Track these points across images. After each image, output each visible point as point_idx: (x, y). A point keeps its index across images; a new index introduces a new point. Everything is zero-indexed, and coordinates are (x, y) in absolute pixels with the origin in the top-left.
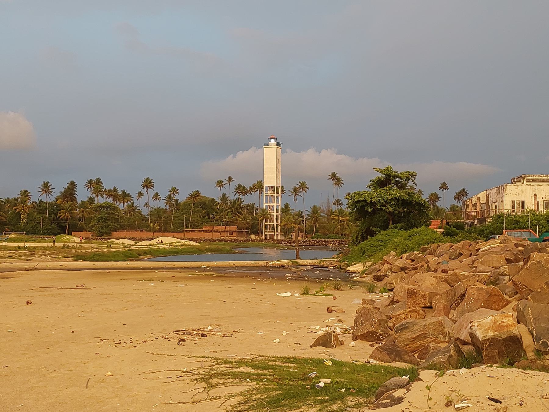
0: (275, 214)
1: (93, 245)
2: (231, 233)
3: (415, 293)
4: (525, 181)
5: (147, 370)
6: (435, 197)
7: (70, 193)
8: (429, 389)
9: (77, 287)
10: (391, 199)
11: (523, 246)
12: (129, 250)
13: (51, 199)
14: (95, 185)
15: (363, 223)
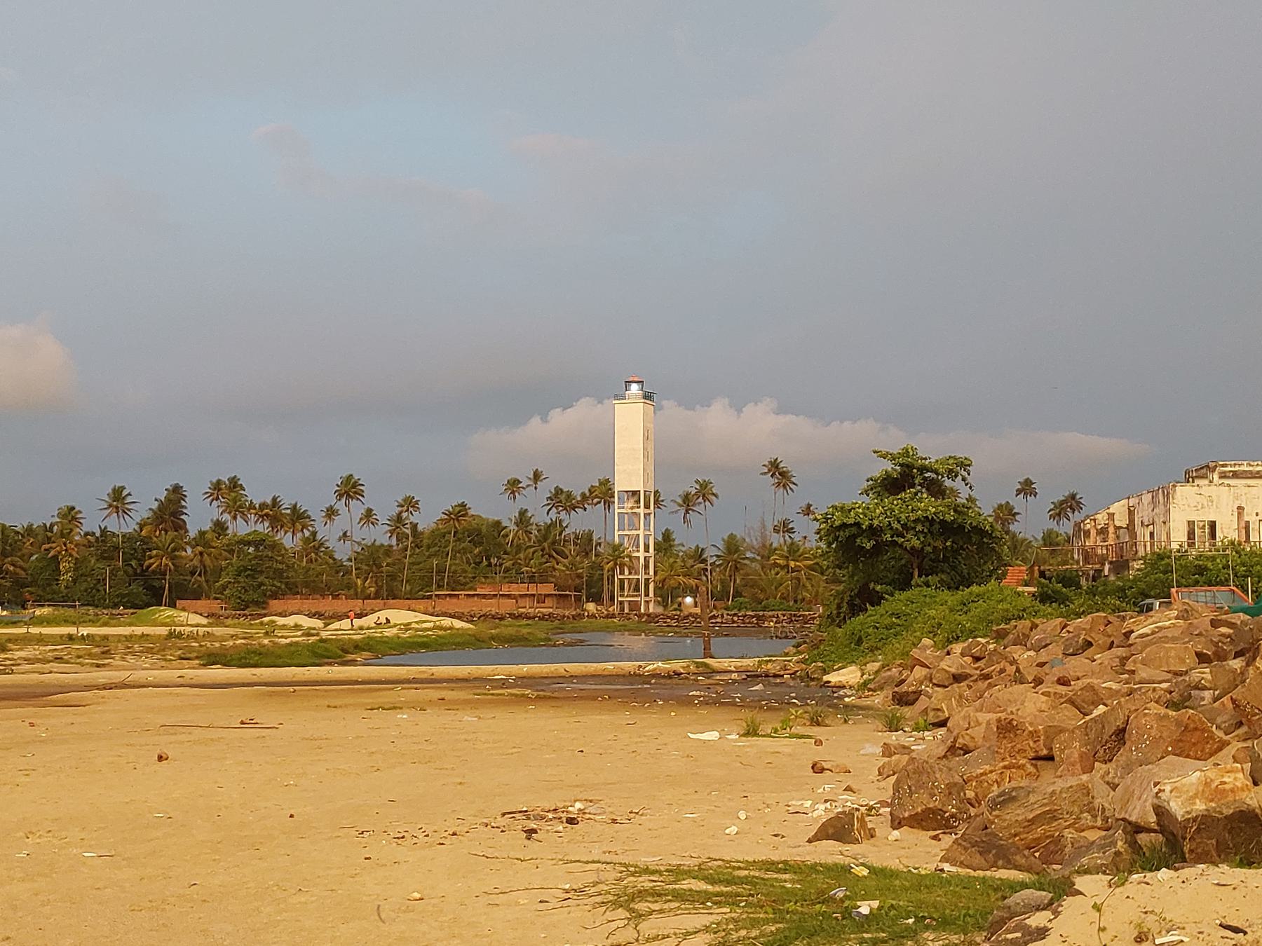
0: (641, 554)
1: (231, 631)
2: (541, 599)
3: (1015, 728)
4: (1216, 476)
5: (490, 889)
6: (1006, 513)
7: (171, 511)
8: (1099, 910)
9: (242, 723)
10: (917, 521)
11: (1231, 625)
12: (171, 635)
13: (123, 526)
14: (228, 491)
15: (852, 576)
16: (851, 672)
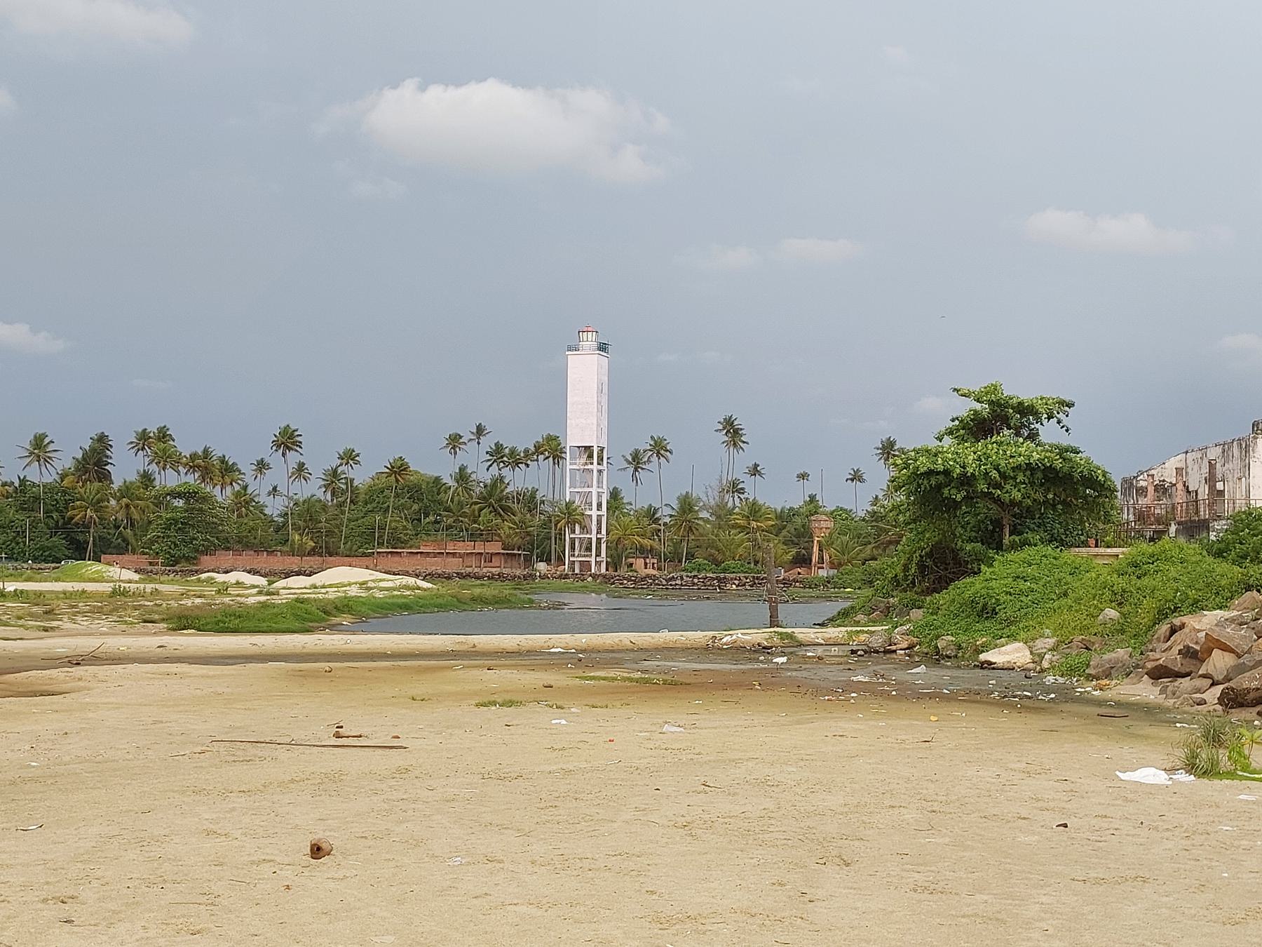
7: (95, 462)
10: (1019, 467)
12: (114, 593)
14: (155, 443)
16: (1017, 650)
